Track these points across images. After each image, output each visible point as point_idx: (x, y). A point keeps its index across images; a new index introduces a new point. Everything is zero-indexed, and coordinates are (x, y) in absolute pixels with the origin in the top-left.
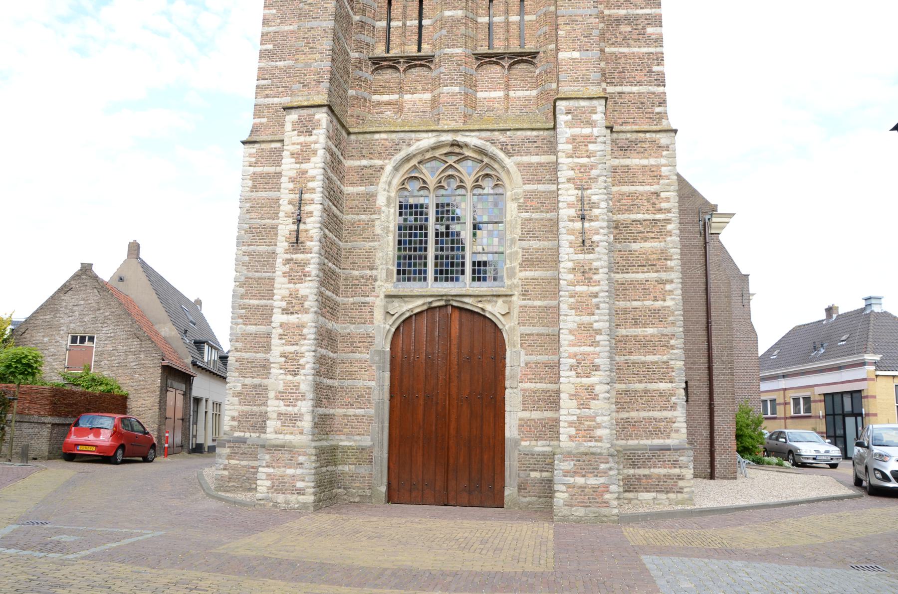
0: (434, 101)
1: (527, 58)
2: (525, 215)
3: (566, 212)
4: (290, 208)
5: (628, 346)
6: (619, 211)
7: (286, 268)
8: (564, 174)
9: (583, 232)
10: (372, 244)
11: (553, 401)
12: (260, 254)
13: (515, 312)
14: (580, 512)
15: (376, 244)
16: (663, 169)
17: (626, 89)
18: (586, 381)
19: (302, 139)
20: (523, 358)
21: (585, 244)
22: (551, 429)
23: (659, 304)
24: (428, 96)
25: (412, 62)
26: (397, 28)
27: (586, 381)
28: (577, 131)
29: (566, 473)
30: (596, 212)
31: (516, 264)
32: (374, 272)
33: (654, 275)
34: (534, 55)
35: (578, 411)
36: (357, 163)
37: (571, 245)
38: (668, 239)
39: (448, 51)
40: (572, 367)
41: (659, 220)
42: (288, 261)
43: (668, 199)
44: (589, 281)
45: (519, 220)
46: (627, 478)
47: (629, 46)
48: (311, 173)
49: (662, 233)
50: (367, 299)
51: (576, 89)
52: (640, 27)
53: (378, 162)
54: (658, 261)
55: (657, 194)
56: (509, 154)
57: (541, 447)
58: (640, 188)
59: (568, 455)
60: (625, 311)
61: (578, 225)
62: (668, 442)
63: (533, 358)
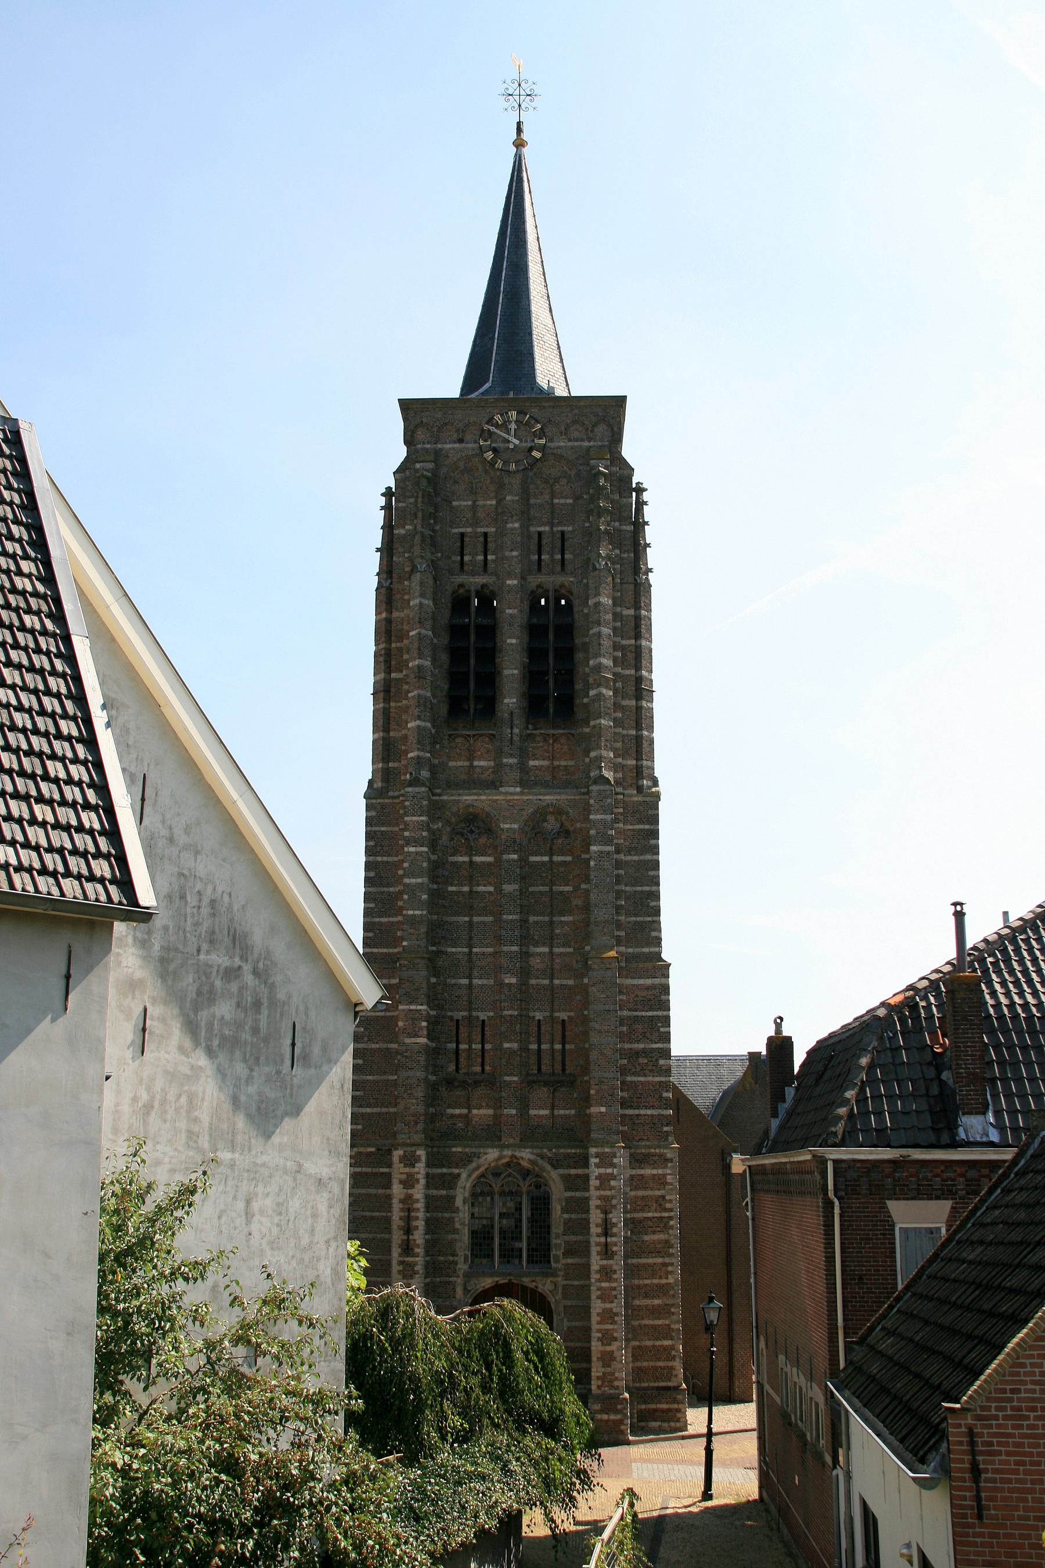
0: (496, 1117)
2: (566, 1216)
3: (595, 1230)
5: (640, 1313)
6: (635, 1210)
7: (401, 1268)
8: (594, 1203)
9: (606, 1244)
10: (453, 1236)
15: (456, 1236)
16: (668, 1177)
17: (643, 1112)
18: (608, 1348)
19: (407, 1170)
20: (566, 1323)
24: (491, 1112)
26: (465, 1050)
27: (608, 1348)
28: (602, 1170)
31: (560, 1253)
32: (456, 1259)
33: (660, 1260)
35: (603, 1370)
37: (598, 1253)
38: (671, 1232)
39: (507, 1078)
40: (599, 1339)
41: (664, 1217)
43: (670, 1201)
44: (610, 1279)
45: (562, 1220)
46: (640, 1412)
47: (645, 1076)
50: (451, 1279)
51: (603, 1136)
52: (654, 1059)
53: (456, 1171)
55: (663, 1197)
56: (555, 1167)
58: (650, 1193)
60: (639, 1287)
61: (603, 1239)
62: (670, 1384)
63: (573, 1324)
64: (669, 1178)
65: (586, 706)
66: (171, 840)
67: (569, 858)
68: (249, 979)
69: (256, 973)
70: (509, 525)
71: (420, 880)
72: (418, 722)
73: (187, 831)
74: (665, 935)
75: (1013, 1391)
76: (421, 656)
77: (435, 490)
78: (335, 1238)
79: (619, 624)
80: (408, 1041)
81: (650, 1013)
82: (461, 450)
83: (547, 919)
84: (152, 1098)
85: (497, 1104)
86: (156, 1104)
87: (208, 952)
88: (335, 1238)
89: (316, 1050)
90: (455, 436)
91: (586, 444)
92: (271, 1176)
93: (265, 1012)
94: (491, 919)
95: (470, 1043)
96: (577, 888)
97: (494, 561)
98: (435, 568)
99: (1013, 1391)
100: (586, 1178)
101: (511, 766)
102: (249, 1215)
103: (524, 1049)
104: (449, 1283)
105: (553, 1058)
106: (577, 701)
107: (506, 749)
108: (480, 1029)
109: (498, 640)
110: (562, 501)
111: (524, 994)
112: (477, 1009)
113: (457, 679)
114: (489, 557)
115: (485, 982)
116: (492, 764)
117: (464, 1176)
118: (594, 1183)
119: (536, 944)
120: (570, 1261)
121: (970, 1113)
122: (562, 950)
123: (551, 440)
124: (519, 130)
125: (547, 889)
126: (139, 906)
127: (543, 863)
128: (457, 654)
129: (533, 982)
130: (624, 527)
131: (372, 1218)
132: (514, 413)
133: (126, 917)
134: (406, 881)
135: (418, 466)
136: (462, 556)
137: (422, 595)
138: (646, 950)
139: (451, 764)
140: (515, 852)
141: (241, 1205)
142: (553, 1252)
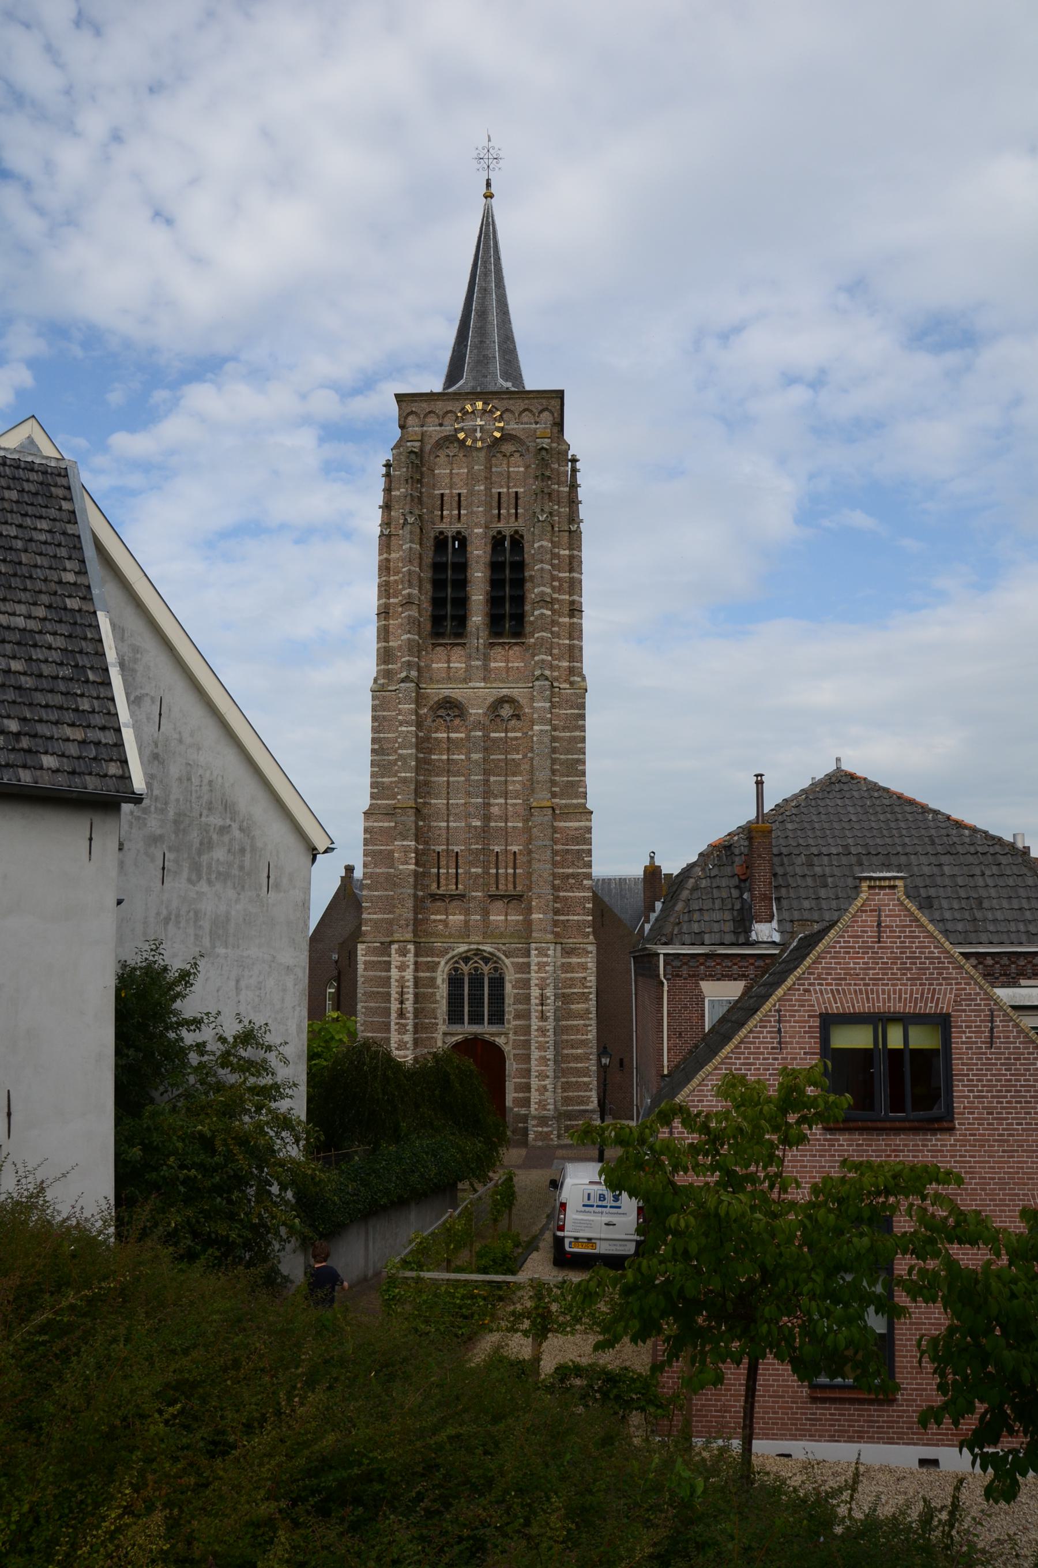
0: (466, 922)
1: (519, 898)
4: (397, 996)
8: (533, 982)
9: (542, 1011)
11: (527, 1088)
12: (371, 1008)
13: (511, 1042)
14: (540, 1143)
17: (571, 918)
19: (401, 959)
20: (515, 1066)
21: (543, 1017)
22: (526, 1102)
23: (585, 1037)
24: (462, 917)
25: (453, 898)
28: (540, 959)
29: (534, 1126)
30: (549, 1001)
31: (511, 1017)
34: (521, 896)
36: (425, 959)
39: (473, 894)
42: (397, 1024)
44: (545, 1036)
48: (407, 977)
49: (587, 1000)
53: (437, 959)
54: (584, 1015)
55: (585, 978)
56: (507, 957)
57: (523, 1111)
58: (576, 975)
59: (535, 1117)
60: (567, 1041)
64: (590, 965)
65: (532, 623)
66: (181, 741)
67: (519, 735)
68: (237, 833)
69: (241, 829)
70: (476, 488)
71: (410, 751)
72: (409, 636)
73: (192, 735)
74: (589, 791)
75: (699, 1101)
76: (410, 586)
77: (421, 461)
78: (299, 1005)
79: (556, 562)
80: (401, 867)
81: (577, 847)
82: (441, 432)
83: (503, 779)
84: (170, 914)
85: (467, 912)
86: (173, 917)
87: (207, 816)
88: (299, 1005)
89: (285, 881)
90: (437, 421)
91: (534, 426)
92: (253, 964)
93: (248, 856)
94: (463, 779)
95: (448, 868)
96: (525, 756)
97: (465, 515)
98: (421, 521)
99: (699, 1101)
100: (528, 965)
101: (477, 667)
102: (238, 989)
103: (486, 872)
104: (432, 1038)
105: (507, 880)
106: (526, 619)
107: (474, 655)
108: (454, 859)
109: (468, 574)
110: (516, 469)
111: (485, 833)
112: (452, 845)
113: (437, 602)
114: (462, 512)
115: (458, 824)
116: (464, 665)
117: (443, 963)
118: (534, 968)
119: (496, 797)
120: (518, 1023)
121: (761, 922)
122: (514, 801)
123: (508, 424)
124: (488, 184)
125: (503, 757)
126: (134, 793)
127: (501, 739)
128: (438, 584)
129: (492, 824)
130: (562, 489)
131: (378, 993)
132: (480, 403)
133: (129, 800)
134: (400, 751)
135: (409, 444)
136: (442, 511)
137: (411, 541)
138: (575, 801)
139: (434, 665)
140: (480, 730)
141: (232, 983)
142: (506, 1017)
